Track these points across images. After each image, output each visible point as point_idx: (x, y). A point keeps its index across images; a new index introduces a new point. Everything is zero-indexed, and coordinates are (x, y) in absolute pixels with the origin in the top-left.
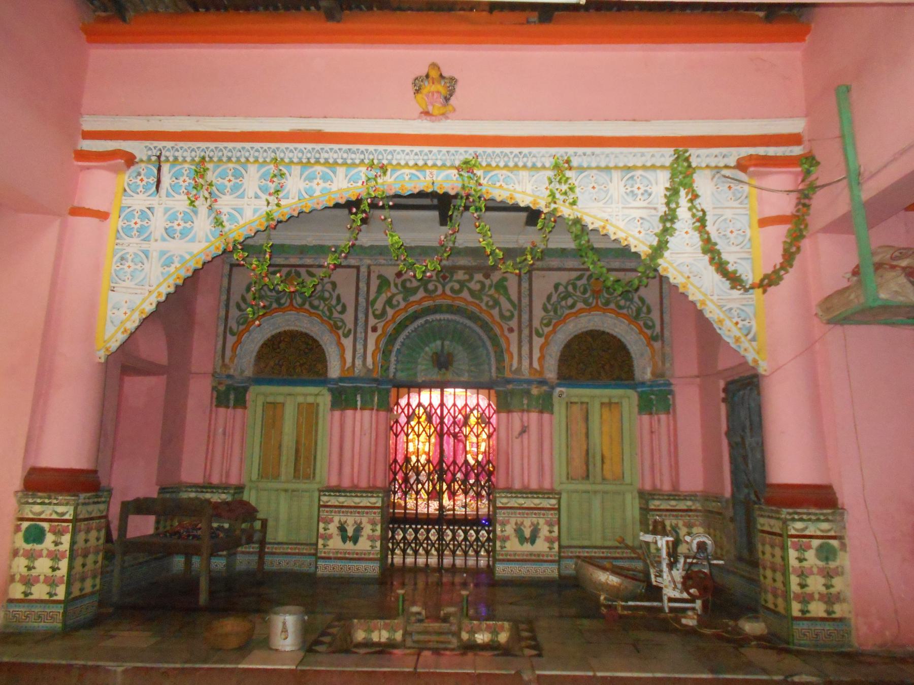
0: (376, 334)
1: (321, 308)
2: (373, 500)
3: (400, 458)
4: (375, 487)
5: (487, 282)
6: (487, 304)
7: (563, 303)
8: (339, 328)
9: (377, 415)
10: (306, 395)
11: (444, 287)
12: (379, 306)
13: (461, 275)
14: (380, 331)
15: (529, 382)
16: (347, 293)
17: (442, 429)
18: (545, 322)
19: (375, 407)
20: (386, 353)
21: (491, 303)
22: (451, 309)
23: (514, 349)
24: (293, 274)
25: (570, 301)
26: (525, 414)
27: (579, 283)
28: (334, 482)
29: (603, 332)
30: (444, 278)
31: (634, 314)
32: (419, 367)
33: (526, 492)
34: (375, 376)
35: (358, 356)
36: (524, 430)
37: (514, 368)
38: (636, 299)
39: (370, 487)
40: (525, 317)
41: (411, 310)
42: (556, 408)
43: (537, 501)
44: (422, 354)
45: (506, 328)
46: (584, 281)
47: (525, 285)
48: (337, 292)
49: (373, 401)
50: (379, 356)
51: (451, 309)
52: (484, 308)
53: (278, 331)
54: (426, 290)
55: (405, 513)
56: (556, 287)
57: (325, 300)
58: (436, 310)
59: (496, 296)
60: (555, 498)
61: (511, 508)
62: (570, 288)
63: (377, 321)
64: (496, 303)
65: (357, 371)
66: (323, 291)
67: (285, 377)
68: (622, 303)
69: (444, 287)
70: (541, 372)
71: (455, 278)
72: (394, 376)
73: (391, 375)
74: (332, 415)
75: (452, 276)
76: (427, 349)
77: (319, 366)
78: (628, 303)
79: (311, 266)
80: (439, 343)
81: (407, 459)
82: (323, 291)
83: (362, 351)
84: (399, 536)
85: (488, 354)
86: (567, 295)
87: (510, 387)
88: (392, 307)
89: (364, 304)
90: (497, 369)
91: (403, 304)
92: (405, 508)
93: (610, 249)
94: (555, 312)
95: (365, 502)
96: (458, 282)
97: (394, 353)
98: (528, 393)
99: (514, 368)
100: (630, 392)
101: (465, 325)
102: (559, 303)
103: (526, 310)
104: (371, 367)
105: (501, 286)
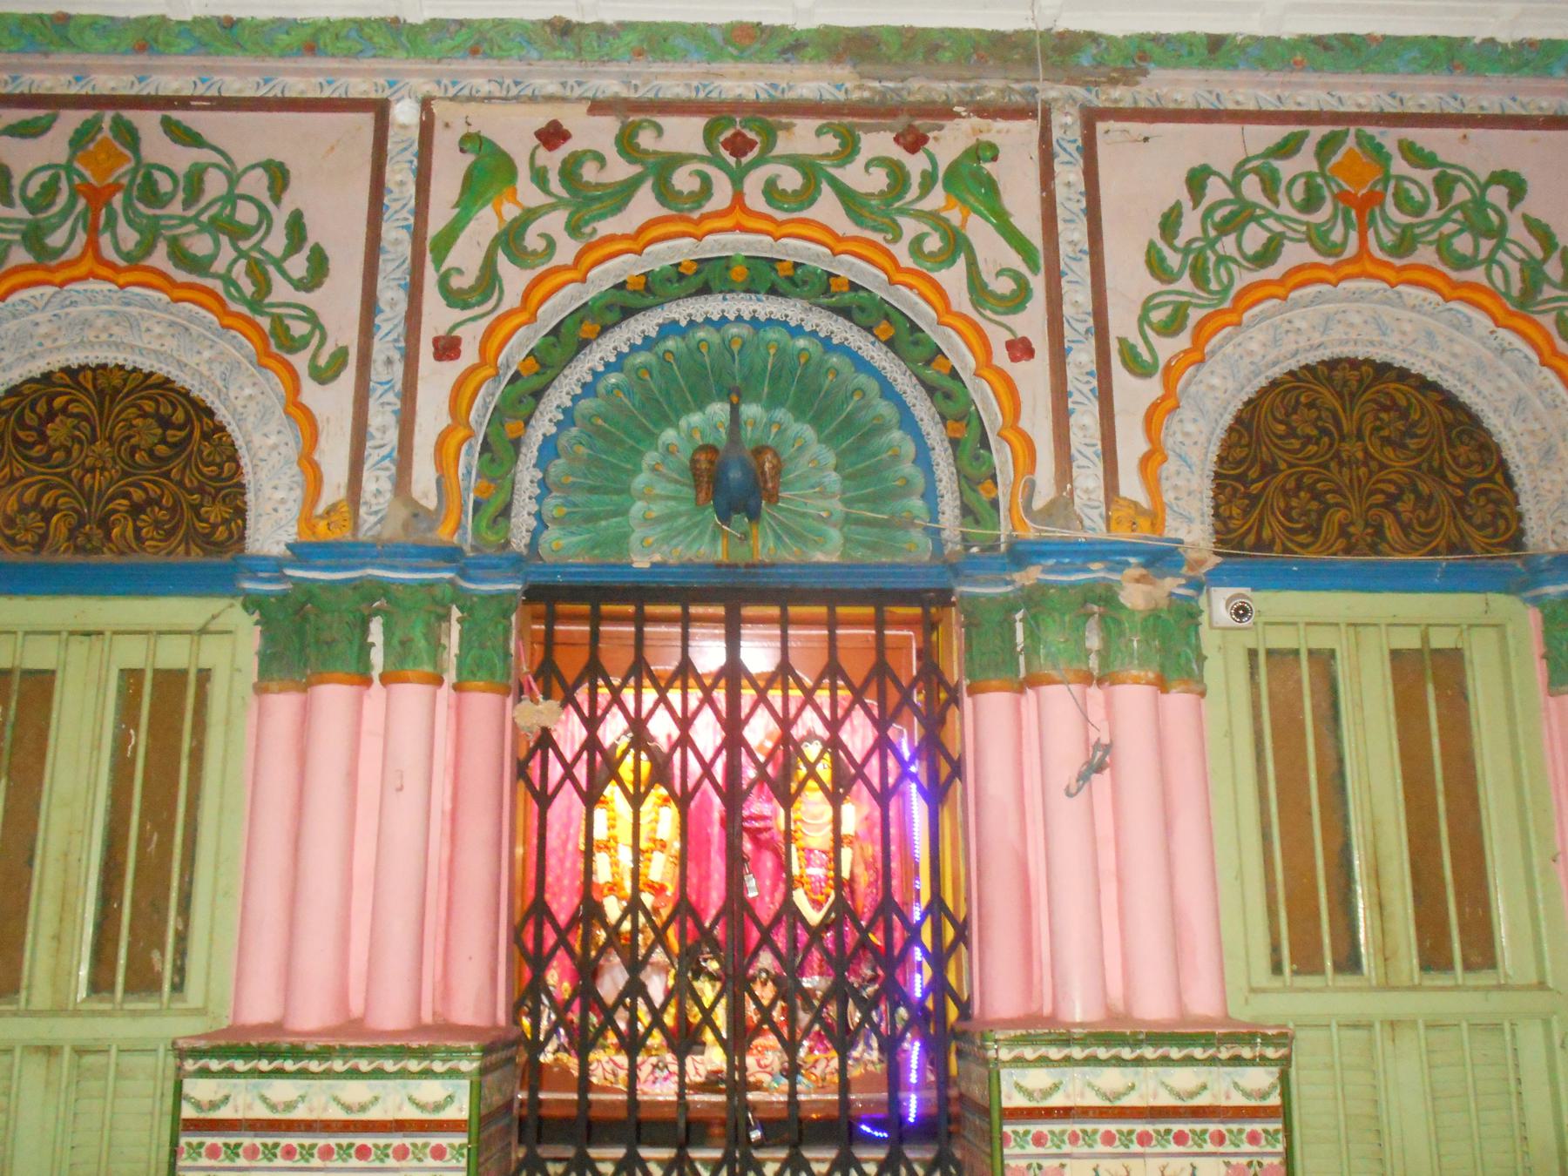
0: (451, 371)
1: (219, 266)
2: (431, 1090)
3: (563, 905)
4: (447, 1029)
5: (916, 165)
6: (917, 244)
7: (1228, 245)
8: (294, 345)
9: (459, 711)
10: (154, 634)
11: (737, 179)
12: (466, 257)
13: (803, 137)
14: (470, 353)
15: (1111, 553)
16: (337, 222)
17: (733, 770)
18: (1157, 316)
19: (450, 677)
20: (498, 451)
21: (933, 243)
22: (769, 277)
23: (1038, 423)
24: (106, 132)
25: (1254, 238)
26: (1095, 693)
27: (1286, 168)
28: (260, 1009)
29: (1383, 370)
30: (739, 146)
31: (1516, 287)
32: (638, 507)
33: (1117, 1038)
34: (444, 534)
35: (372, 456)
36: (1099, 761)
37: (1038, 503)
38: (1516, 230)
39: (421, 1029)
40: (1077, 297)
41: (604, 277)
42: (1213, 672)
43: (1184, 1078)
44: (651, 458)
45: (998, 339)
46: (1305, 161)
47: (1069, 175)
48: (290, 201)
49: (436, 646)
50: (468, 459)
51: (769, 277)
52: (906, 261)
53: (37, 368)
54: (665, 193)
55: (584, 1104)
56: (1197, 181)
57: (238, 232)
58: (705, 278)
59: (954, 216)
60: (1263, 1061)
61: (1066, 1113)
62: (1251, 188)
63: (457, 315)
64: (956, 244)
65: (368, 520)
66: (232, 198)
67: (62, 558)
68: (1463, 244)
69: (737, 179)
70: (1155, 517)
71: (783, 146)
72: (533, 545)
73: (520, 542)
74: (262, 713)
75: (770, 143)
76: (669, 435)
77: (215, 512)
78: (1486, 245)
79: (184, 103)
80: (719, 410)
81: (590, 910)
82: (232, 198)
83: (393, 436)
84: (709, 654)
85: (923, 458)
86: (1239, 218)
87: (1032, 575)
88: (519, 255)
89: (406, 249)
90: (966, 511)
91: (568, 248)
92: (584, 1084)
93: (1399, 40)
94: (1200, 278)
95: (392, 1100)
96: (795, 161)
97: (530, 453)
98: (1107, 597)
99: (1038, 503)
100: (1503, 604)
101: (826, 343)
102: (1212, 244)
103: (1076, 275)
104: (431, 503)
105: (972, 177)
